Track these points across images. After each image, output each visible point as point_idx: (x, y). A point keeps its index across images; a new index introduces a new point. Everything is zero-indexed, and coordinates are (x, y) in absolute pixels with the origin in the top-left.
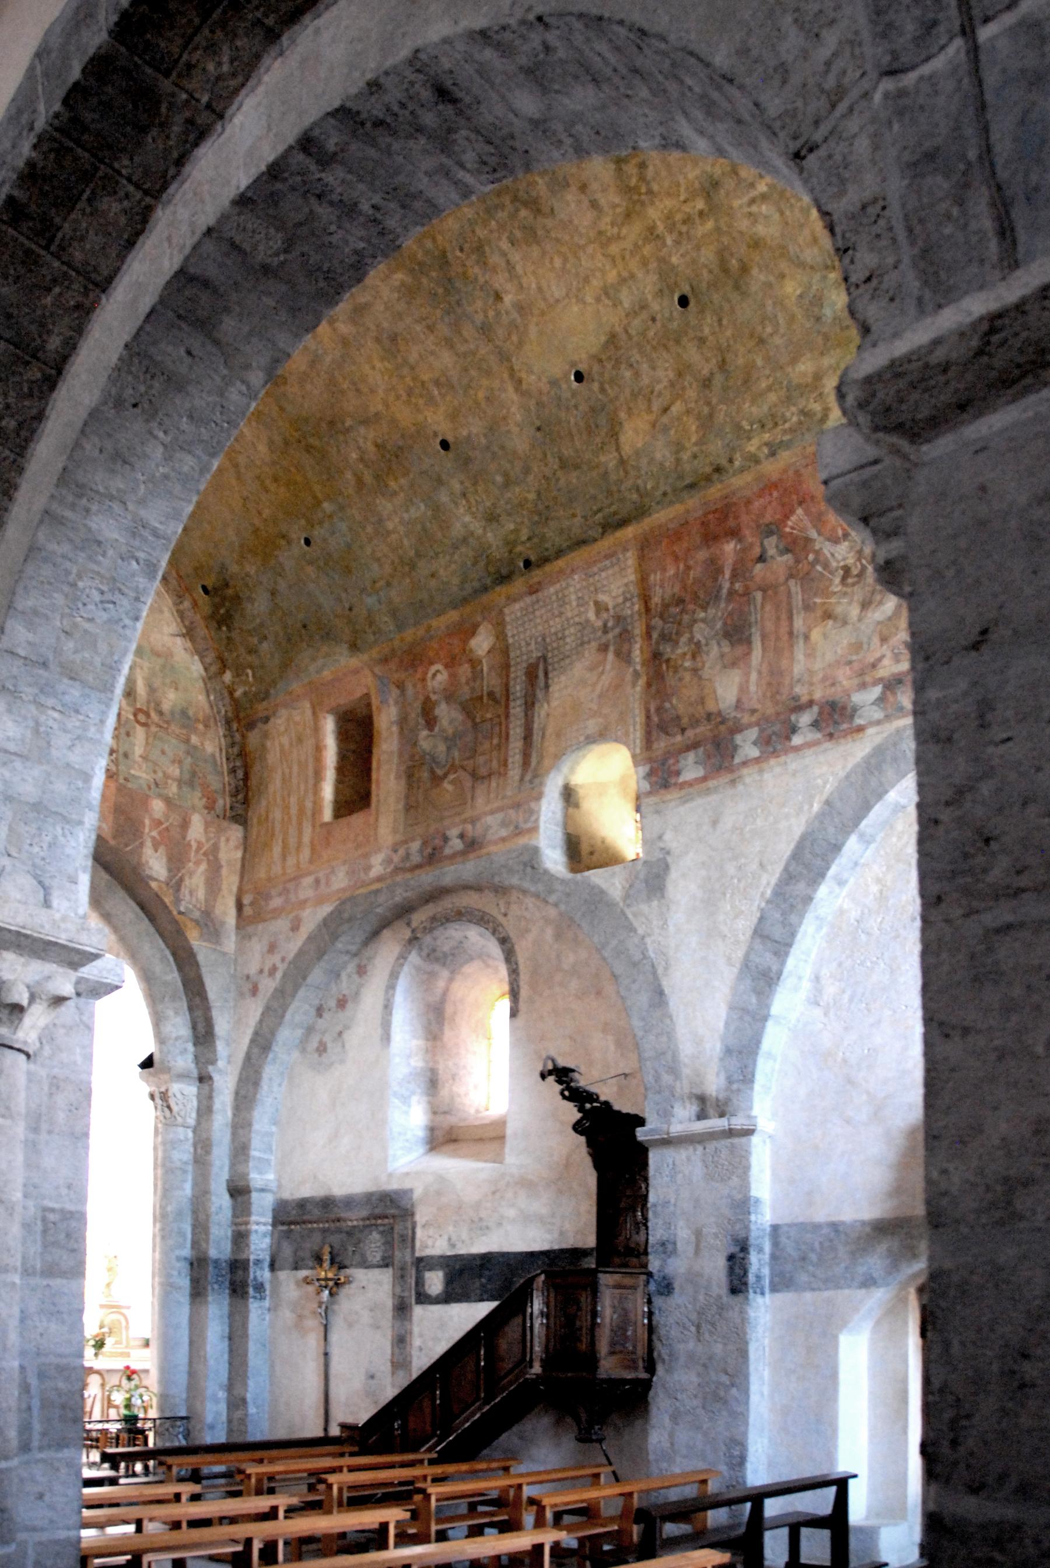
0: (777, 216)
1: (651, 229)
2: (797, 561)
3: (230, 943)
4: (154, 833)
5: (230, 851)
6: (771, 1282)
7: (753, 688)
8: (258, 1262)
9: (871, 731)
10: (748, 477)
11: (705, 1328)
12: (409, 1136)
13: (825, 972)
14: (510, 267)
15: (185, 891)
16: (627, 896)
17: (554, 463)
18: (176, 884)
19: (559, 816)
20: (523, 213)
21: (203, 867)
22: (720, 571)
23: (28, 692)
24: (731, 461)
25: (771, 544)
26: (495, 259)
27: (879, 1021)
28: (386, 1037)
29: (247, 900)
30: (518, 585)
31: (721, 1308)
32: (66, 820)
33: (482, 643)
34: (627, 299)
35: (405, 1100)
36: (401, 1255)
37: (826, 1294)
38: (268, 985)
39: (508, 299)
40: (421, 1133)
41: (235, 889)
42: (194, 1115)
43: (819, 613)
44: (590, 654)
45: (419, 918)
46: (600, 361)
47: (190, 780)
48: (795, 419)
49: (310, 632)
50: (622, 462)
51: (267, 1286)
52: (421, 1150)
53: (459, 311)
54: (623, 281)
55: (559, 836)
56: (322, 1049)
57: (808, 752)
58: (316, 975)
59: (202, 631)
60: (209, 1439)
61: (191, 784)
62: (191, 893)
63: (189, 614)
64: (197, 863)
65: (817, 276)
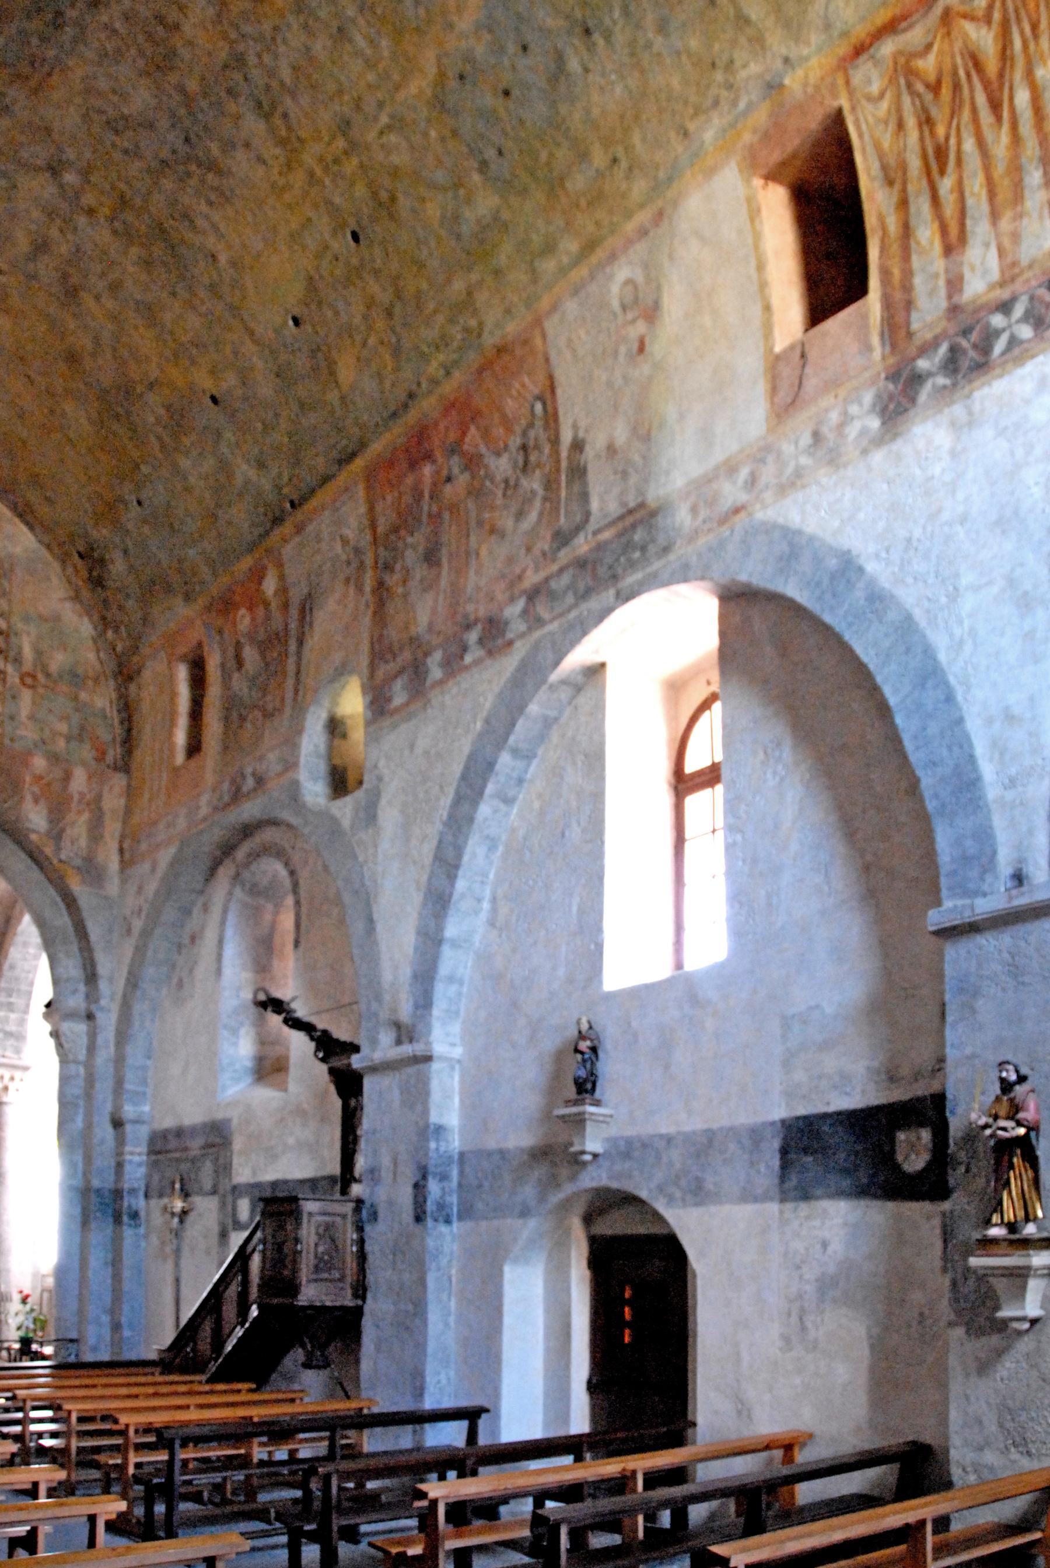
0: (404, 144)
1: (311, 174)
2: (473, 478)
3: (113, 888)
4: (36, 789)
5: (113, 801)
6: (459, 1211)
7: (440, 609)
8: (133, 1191)
9: (518, 644)
10: (433, 400)
12: (237, 1066)
13: (500, 893)
14: (215, 228)
15: (66, 843)
16: (352, 827)
17: (295, 407)
18: (57, 835)
19: (322, 748)
20: (210, 176)
21: (86, 816)
22: (421, 494)
24: (419, 384)
25: (455, 462)
26: (200, 222)
27: (535, 943)
28: (219, 972)
29: (125, 846)
30: (287, 528)
33: (270, 586)
34: (311, 243)
35: (234, 1032)
36: (225, 1186)
37: (496, 1223)
38: (138, 924)
39: (223, 259)
40: (249, 1064)
41: (117, 834)
42: (84, 1052)
43: (487, 527)
44: (339, 587)
45: (241, 854)
47: (80, 734)
48: (459, 337)
49: (155, 587)
50: (343, 398)
51: (142, 1214)
52: (249, 1080)
53: (189, 275)
55: (322, 768)
56: (180, 985)
57: (475, 670)
58: (169, 914)
59: (85, 594)
60: (89, 1357)
61: (80, 738)
62: (72, 843)
63: (74, 579)
64: (80, 813)
65: (450, 194)
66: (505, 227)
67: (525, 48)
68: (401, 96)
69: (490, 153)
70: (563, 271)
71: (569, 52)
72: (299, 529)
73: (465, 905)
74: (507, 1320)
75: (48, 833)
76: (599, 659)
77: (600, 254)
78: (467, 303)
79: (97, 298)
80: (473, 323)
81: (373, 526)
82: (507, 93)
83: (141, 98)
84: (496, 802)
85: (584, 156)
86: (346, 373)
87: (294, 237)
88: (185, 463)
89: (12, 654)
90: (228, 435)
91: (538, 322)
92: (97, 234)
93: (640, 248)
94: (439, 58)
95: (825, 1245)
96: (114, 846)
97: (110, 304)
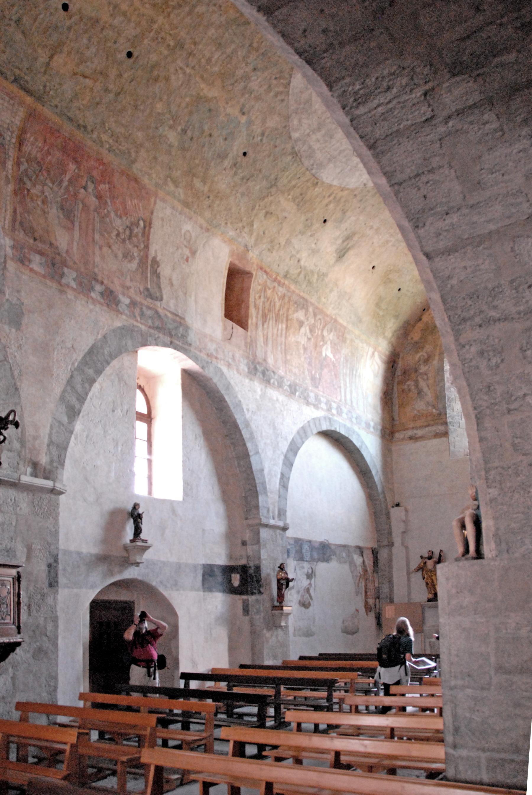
11: (33, 608)
31: (43, 596)
46: (81, 19)
54: (125, 14)
72: (359, 376)
94: (215, 98)
95: (216, 607)
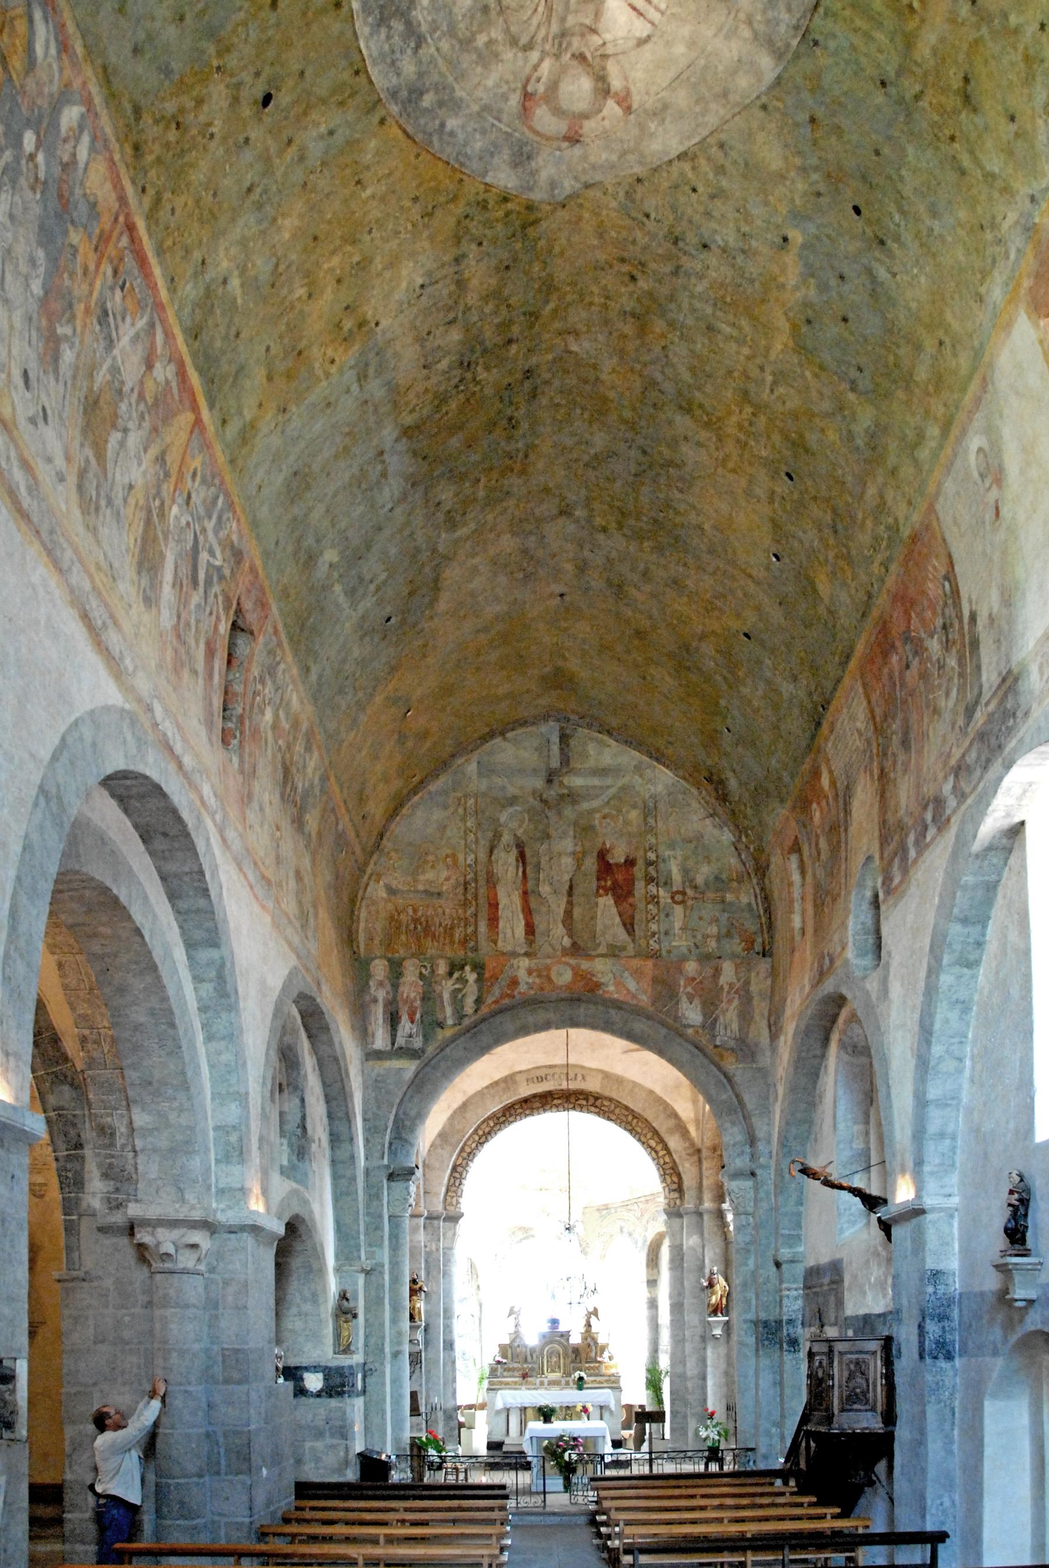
1: (738, 441)
4: (689, 989)
8: (790, 1322)
15: (720, 1029)
18: (710, 1023)
21: (736, 1002)
23: (148, 1099)
26: (682, 507)
32: (187, 1153)
33: (825, 781)
39: (706, 527)
61: (729, 935)
64: (730, 1002)
66: (885, 429)
67: (842, 277)
68: (772, 357)
69: (853, 373)
70: (935, 455)
71: (875, 265)
73: (949, 1065)
74: (988, 1452)
75: (703, 1027)
76: (1017, 820)
77: (955, 432)
78: (881, 507)
79: (638, 588)
80: (890, 520)
81: (873, 718)
82: (845, 320)
83: (600, 440)
84: (957, 969)
85: (918, 347)
86: (824, 587)
87: (748, 493)
88: (746, 691)
89: (662, 880)
90: (767, 662)
91: (931, 509)
92: (615, 543)
93: (979, 420)
96: (764, 1024)
97: (648, 588)
